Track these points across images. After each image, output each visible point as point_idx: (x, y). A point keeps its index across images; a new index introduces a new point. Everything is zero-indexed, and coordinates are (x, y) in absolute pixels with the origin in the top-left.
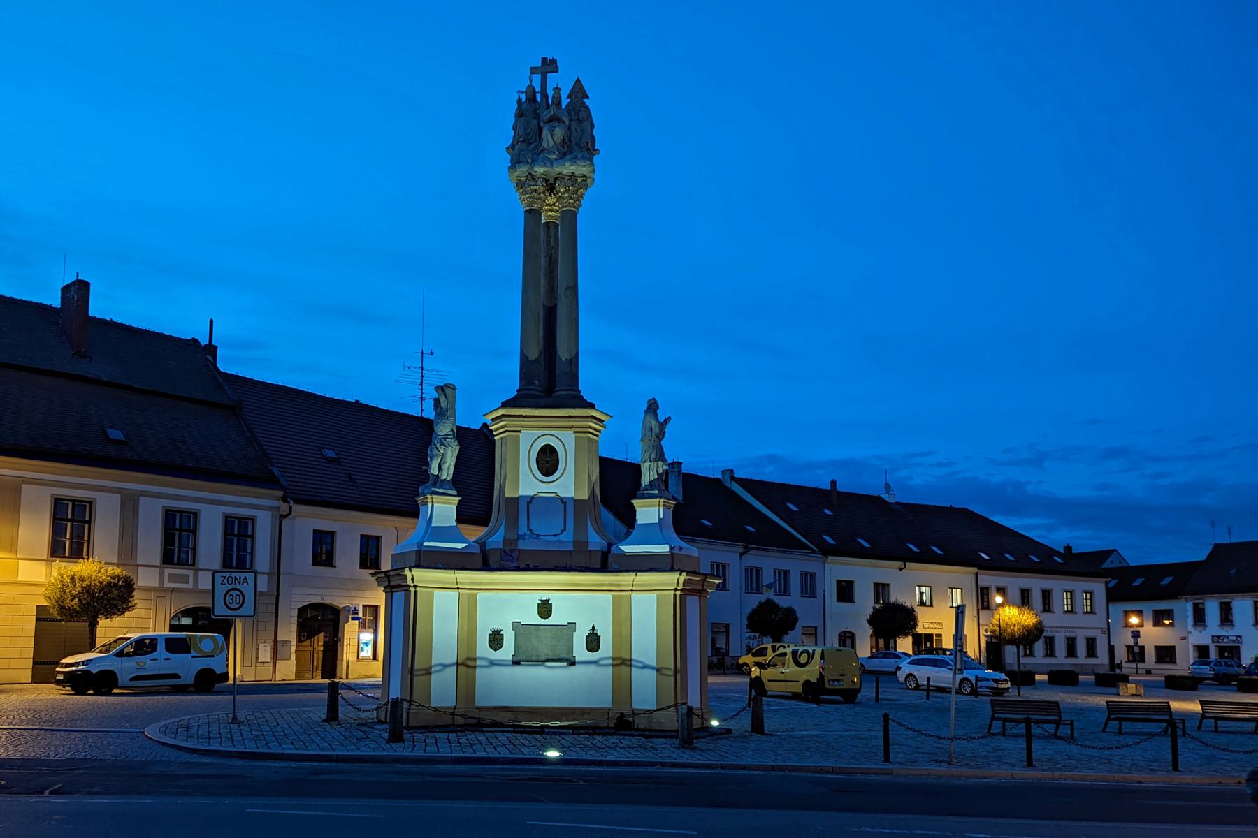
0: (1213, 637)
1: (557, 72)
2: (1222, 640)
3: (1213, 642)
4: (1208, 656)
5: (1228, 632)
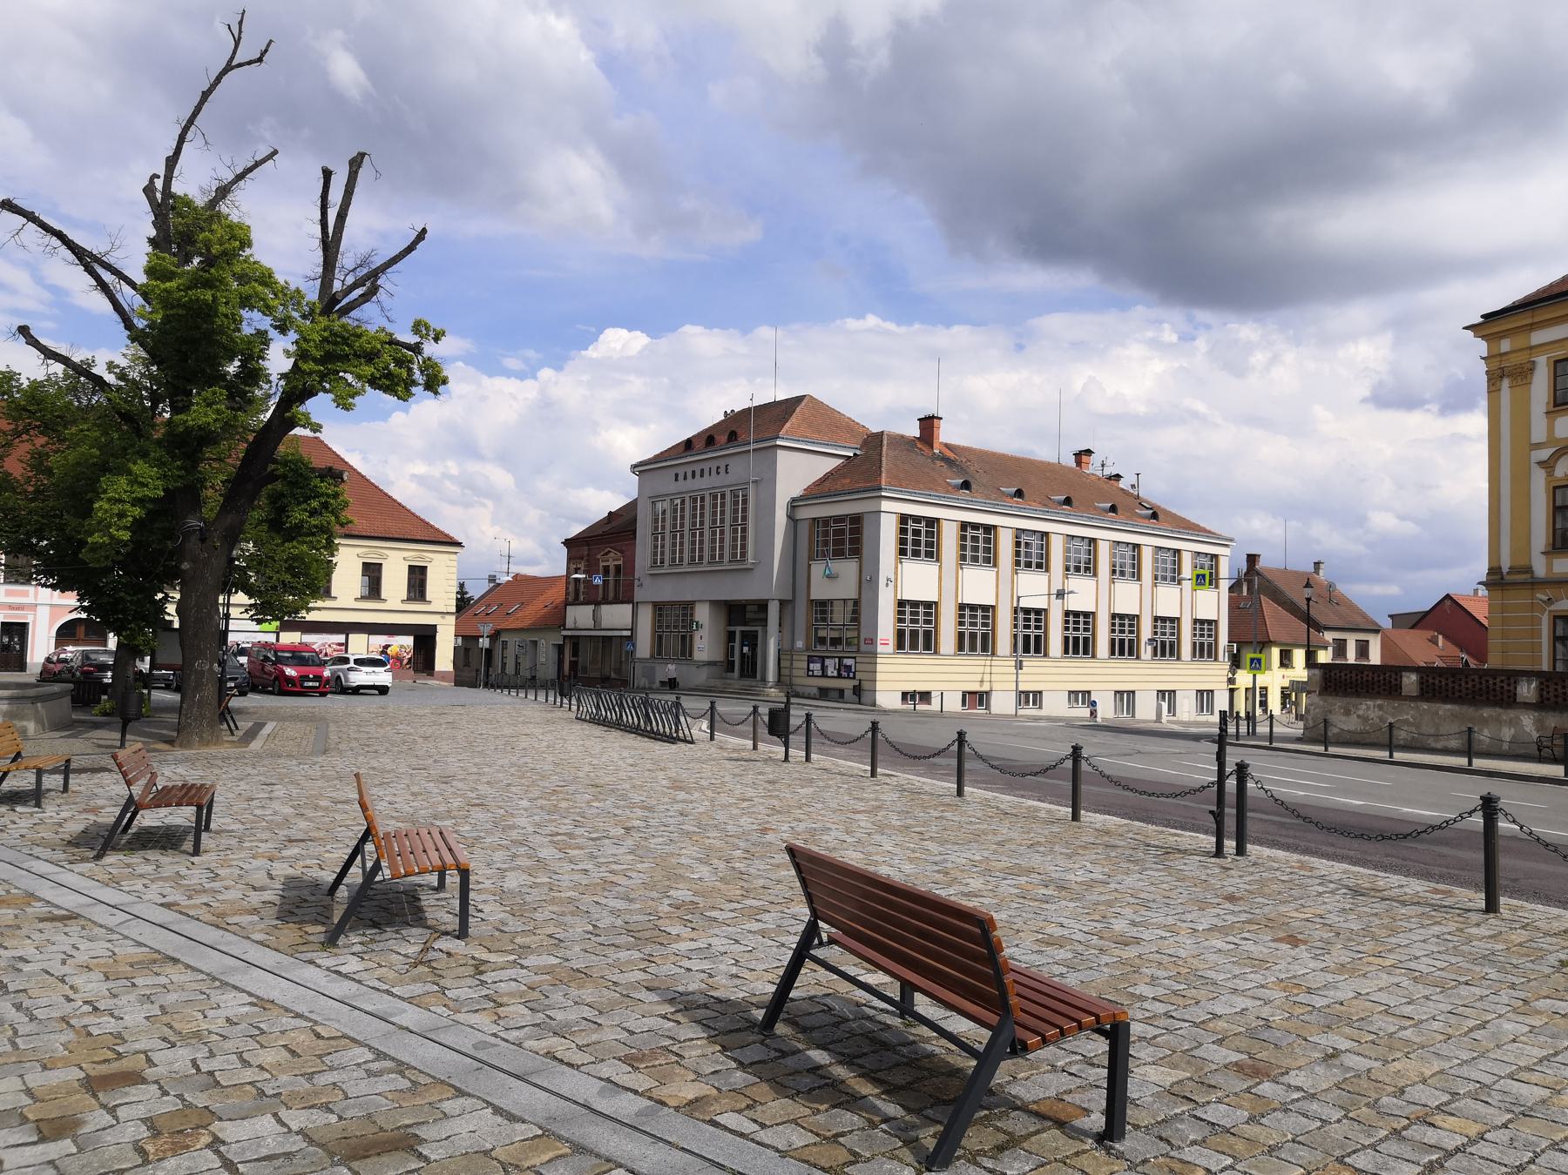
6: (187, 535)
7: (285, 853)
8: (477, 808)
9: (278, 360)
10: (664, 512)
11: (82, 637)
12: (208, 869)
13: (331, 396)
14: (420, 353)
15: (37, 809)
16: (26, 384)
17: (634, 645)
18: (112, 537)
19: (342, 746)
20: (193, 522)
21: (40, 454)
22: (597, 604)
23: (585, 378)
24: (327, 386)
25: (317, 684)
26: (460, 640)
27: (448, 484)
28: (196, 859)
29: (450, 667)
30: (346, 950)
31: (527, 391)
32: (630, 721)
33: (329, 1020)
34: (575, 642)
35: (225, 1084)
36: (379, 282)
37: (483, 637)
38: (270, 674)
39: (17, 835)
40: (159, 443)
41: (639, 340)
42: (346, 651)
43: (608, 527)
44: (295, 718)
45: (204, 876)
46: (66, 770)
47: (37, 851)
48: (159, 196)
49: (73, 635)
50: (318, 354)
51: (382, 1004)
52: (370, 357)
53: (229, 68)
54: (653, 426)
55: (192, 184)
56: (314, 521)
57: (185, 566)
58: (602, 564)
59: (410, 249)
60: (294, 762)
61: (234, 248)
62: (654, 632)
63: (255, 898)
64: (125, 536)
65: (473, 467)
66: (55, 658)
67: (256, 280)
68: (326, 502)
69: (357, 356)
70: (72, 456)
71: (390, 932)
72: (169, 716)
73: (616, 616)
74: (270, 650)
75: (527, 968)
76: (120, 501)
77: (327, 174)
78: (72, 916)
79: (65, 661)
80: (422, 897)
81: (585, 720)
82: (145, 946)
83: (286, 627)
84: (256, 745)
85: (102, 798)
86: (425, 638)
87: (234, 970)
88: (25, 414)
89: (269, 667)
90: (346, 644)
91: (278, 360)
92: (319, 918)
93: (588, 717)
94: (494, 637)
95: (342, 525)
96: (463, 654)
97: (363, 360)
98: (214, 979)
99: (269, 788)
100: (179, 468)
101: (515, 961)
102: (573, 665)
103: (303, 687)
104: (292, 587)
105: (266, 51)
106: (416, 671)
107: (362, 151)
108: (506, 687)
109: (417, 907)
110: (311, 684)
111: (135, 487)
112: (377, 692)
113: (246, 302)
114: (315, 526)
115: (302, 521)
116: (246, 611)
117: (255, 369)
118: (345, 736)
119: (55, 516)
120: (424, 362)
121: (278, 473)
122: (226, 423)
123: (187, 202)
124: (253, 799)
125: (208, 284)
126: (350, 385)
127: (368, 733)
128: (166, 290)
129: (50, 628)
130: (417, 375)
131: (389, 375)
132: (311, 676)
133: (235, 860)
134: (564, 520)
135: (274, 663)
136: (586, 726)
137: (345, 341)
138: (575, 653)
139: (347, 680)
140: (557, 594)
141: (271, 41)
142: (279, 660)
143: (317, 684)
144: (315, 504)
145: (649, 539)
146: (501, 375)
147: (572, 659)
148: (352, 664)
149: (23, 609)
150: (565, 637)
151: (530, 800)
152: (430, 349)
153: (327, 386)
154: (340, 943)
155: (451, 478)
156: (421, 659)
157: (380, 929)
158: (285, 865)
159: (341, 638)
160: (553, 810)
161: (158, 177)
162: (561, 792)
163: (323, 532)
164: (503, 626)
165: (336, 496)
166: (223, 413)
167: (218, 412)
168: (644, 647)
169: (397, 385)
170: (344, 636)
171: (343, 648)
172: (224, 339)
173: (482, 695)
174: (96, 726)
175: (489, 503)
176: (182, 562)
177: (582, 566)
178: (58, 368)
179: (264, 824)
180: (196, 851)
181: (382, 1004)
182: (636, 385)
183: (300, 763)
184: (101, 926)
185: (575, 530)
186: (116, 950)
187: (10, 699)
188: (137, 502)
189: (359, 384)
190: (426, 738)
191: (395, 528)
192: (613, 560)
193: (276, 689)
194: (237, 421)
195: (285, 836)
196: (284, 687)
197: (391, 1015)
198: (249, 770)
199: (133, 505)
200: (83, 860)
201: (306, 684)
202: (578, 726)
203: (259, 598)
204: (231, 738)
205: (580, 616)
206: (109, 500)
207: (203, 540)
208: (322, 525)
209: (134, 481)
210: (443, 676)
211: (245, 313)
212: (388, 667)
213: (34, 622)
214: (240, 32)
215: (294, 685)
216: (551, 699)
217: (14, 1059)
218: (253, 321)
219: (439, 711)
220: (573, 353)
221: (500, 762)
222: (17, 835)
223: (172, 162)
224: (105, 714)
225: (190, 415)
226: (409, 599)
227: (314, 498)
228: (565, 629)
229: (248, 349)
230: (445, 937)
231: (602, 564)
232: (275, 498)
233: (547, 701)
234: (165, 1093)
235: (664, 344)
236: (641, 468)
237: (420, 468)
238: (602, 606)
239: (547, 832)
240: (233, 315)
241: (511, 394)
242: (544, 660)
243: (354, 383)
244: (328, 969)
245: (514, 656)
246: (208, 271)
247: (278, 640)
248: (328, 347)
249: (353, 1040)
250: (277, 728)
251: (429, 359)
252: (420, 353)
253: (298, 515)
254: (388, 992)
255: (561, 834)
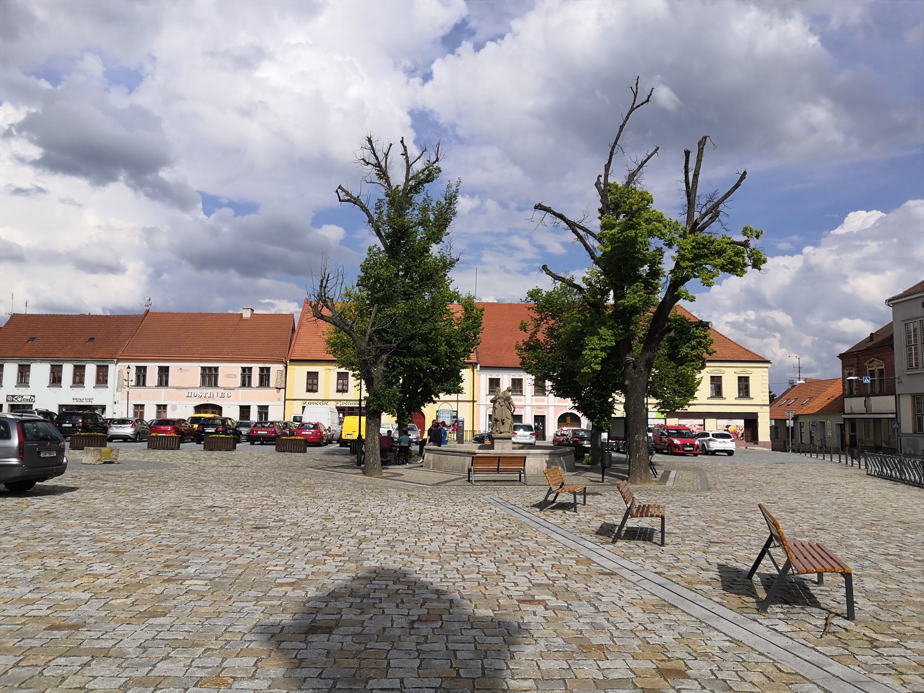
0: (8, 396)
1: (535, 416)
2: (16, 399)
3: (7, 401)
4: (248, 418)
5: (22, 392)
6: (627, 365)
7: (711, 549)
8: (820, 531)
9: (668, 264)
10: (915, 330)
11: (569, 422)
12: (672, 555)
13: (699, 280)
14: (748, 247)
15: (575, 513)
16: (544, 293)
17: (899, 424)
18: (592, 368)
19: (718, 486)
20: (629, 358)
21: (551, 328)
22: (867, 396)
23: (835, 247)
24: (696, 274)
25: (692, 449)
26: (773, 422)
27: (748, 325)
28: (663, 548)
29: (768, 439)
30: (774, 616)
31: (796, 262)
32: (913, 478)
33: (782, 660)
34: (853, 423)
35: (736, 690)
36: (719, 209)
37: (789, 419)
38: (665, 442)
39: (572, 527)
40: (610, 316)
41: (875, 215)
42: (704, 430)
43: (872, 343)
44: (685, 469)
45: (671, 558)
46: (584, 493)
47: (584, 535)
48: (602, 186)
49: (565, 421)
50: (690, 256)
51: (814, 657)
52: (720, 253)
53: (632, 110)
54: (888, 273)
55: (618, 179)
56: (694, 353)
57: (627, 382)
58: (868, 369)
59: (737, 186)
60: (694, 495)
61: (644, 205)
62: (914, 415)
63: (706, 575)
64: (598, 368)
65: (764, 313)
66: (559, 434)
67: (654, 221)
68: (700, 341)
69: (713, 254)
70: (569, 327)
71: (798, 608)
72: (621, 465)
73: (883, 404)
74: (664, 429)
75: (910, 649)
76: (595, 349)
77: (687, 153)
78: (612, 574)
79: (563, 435)
80: (810, 588)
81: (875, 476)
82: (656, 596)
83: (672, 414)
84: (669, 484)
85: (602, 509)
86: (751, 421)
87: (710, 617)
88: (545, 310)
89: (664, 439)
90: (704, 425)
91: (668, 264)
92: (749, 593)
93: (876, 474)
94: (795, 418)
95: (710, 354)
96: (774, 431)
97: (716, 256)
98: (701, 622)
99: (686, 510)
100: (621, 329)
101: (898, 643)
102: (853, 438)
103: (684, 450)
104: (679, 392)
105: (650, 95)
106: (747, 441)
107: (705, 135)
108: (808, 452)
109: (809, 593)
110: (688, 449)
111: (601, 341)
112: (726, 454)
113: (651, 234)
114: (695, 356)
115: (687, 353)
116: (655, 407)
117: (657, 270)
118: (717, 480)
119: (560, 360)
120: (751, 252)
121: (671, 327)
122: (645, 302)
123: (616, 187)
124: (680, 516)
125: (632, 227)
126: (710, 271)
127: (730, 479)
128: (612, 234)
129: (555, 418)
130: (747, 260)
131: (732, 263)
132: (688, 444)
133: (684, 551)
134: (829, 342)
135: (667, 437)
136: (876, 479)
137: (705, 246)
138: (853, 429)
139: (709, 446)
140: (837, 390)
141: (653, 89)
142: (670, 435)
143: (692, 449)
144: (694, 343)
145: (905, 350)
146: (778, 255)
147: (852, 434)
148: (711, 437)
149: (543, 408)
150: (845, 419)
151: (857, 528)
152: (753, 243)
153: (696, 274)
154: (769, 610)
155: (750, 321)
156: (749, 433)
157: (790, 605)
158: (715, 557)
159: (701, 421)
160: (877, 537)
161: (601, 176)
162: (878, 525)
163: (700, 359)
164: (800, 413)
165: (705, 337)
166: (643, 296)
167: (640, 296)
168: (907, 424)
169: (737, 267)
170: (702, 420)
171: (702, 427)
172: (639, 255)
173: (790, 456)
174: (587, 470)
175: (778, 335)
176: (625, 381)
177: (853, 371)
178: (559, 283)
179: (691, 530)
180: (663, 544)
181: (814, 657)
182: (873, 247)
183: (697, 496)
184: (629, 581)
185: (845, 349)
186: (643, 596)
187: (550, 454)
188: (603, 349)
189: (715, 270)
190: (768, 483)
191: (727, 355)
192: (877, 365)
193: (670, 452)
194: (650, 300)
195: (707, 539)
196: (673, 450)
197: (823, 665)
198: (671, 498)
199: (601, 351)
200: (607, 543)
201: (686, 449)
202: (870, 480)
203: (662, 399)
204: (655, 479)
205: (855, 405)
206: (590, 349)
207: (635, 368)
208: (698, 355)
209: (600, 339)
210: (764, 444)
211: (650, 240)
212: (733, 439)
213: (525, 414)
214: (637, 88)
215: (679, 449)
216: (843, 461)
217: (617, 650)
218: (655, 243)
219: (770, 467)
220: (825, 233)
221: (824, 501)
222: (572, 527)
223: (607, 167)
224: (589, 464)
225: (625, 300)
226: (740, 397)
227: (693, 339)
228: (844, 414)
229: (653, 259)
230: (838, 618)
231: (868, 369)
232: (671, 341)
233: (840, 462)
234: (703, 688)
235: (893, 216)
236: (893, 302)
237: (732, 317)
238: (871, 398)
239: (880, 552)
240: (645, 241)
241: (784, 266)
242: (831, 434)
243: (712, 270)
244: (767, 626)
245: (809, 432)
246: (632, 220)
247: (666, 423)
248: (695, 251)
249: (807, 679)
250: (678, 474)
251: (754, 249)
252: (748, 247)
253: (685, 350)
254: (813, 648)
255: (891, 555)
